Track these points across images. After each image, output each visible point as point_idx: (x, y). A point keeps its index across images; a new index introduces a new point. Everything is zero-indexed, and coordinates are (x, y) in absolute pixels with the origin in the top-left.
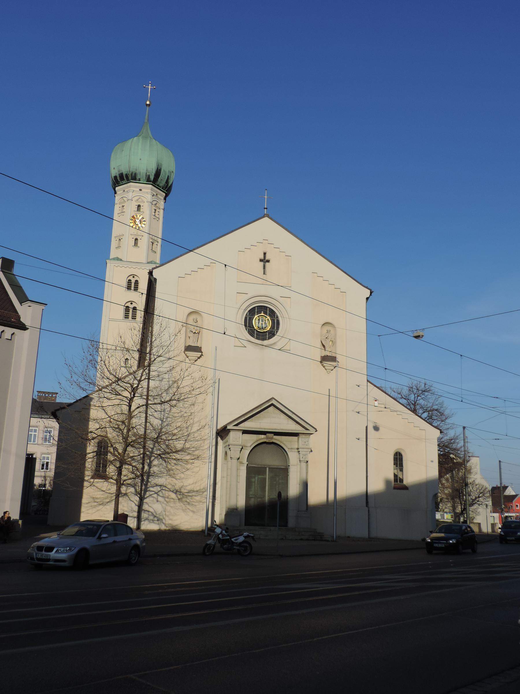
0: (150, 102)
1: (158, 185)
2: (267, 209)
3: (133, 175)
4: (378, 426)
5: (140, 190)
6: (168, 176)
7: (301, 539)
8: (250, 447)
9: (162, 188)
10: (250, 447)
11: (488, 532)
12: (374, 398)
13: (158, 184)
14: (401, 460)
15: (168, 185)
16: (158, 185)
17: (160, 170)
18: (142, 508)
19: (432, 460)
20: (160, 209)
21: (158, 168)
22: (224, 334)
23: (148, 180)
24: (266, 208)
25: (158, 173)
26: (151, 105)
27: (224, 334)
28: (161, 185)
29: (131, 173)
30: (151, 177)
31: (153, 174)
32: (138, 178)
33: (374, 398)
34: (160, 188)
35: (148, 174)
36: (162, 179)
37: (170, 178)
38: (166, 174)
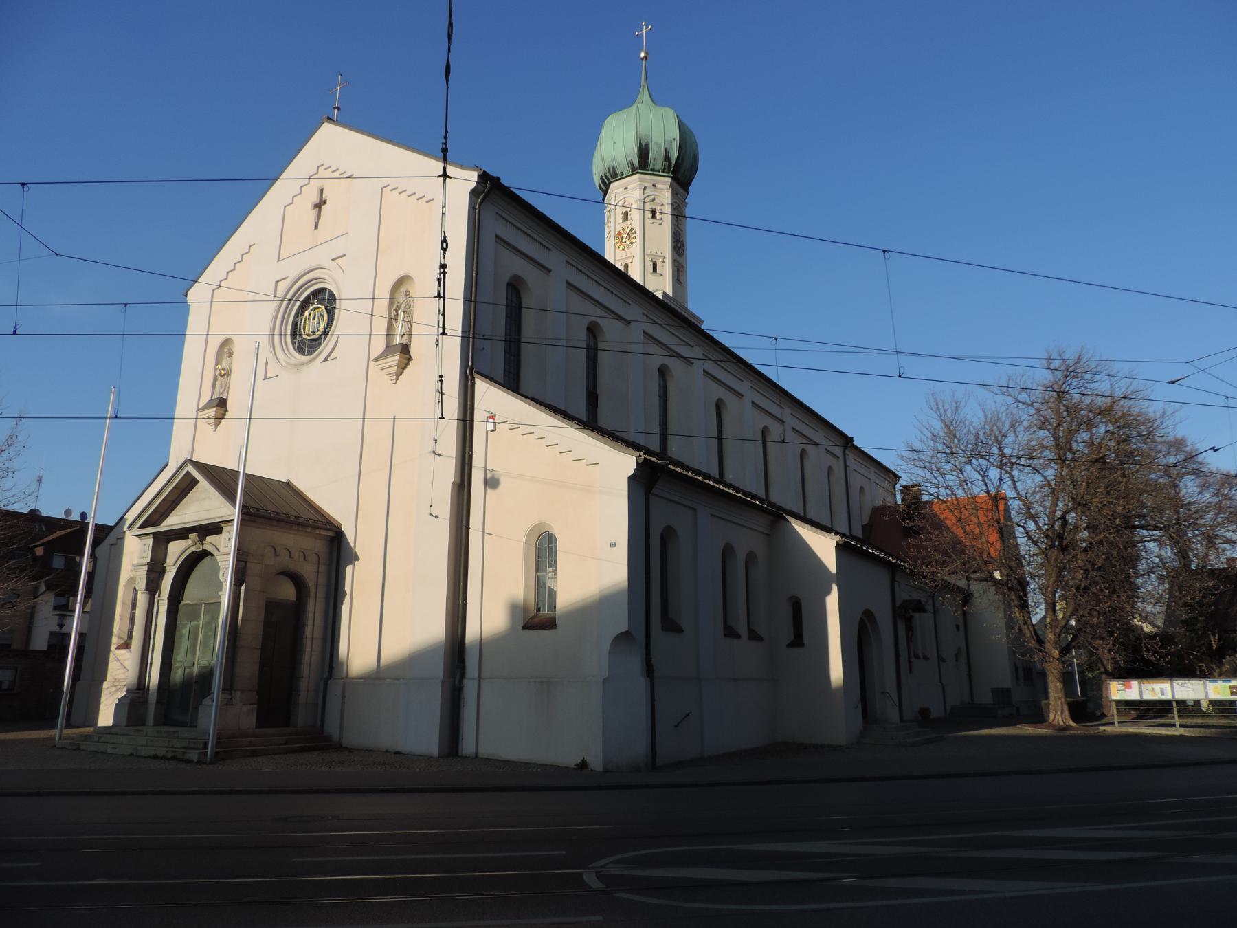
0: (646, 53)
1: (653, 170)
2: (339, 111)
3: (611, 170)
4: (496, 477)
5: (626, 188)
6: (666, 149)
7: (155, 757)
8: (174, 565)
9: (662, 172)
10: (174, 565)
11: (476, 753)
12: (488, 412)
13: (651, 167)
14: (552, 552)
15: (670, 163)
16: (653, 170)
17: (647, 145)
18: (1107, 697)
19: (613, 541)
20: (662, 205)
21: (640, 144)
22: (900, 376)
23: (634, 171)
24: (338, 109)
25: (643, 152)
26: (648, 58)
27: (900, 376)
28: (658, 167)
29: (607, 169)
30: (634, 162)
31: (636, 156)
32: (618, 173)
33: (488, 412)
34: (657, 173)
35: (629, 160)
36: (656, 158)
37: (671, 150)
38: (660, 147)
